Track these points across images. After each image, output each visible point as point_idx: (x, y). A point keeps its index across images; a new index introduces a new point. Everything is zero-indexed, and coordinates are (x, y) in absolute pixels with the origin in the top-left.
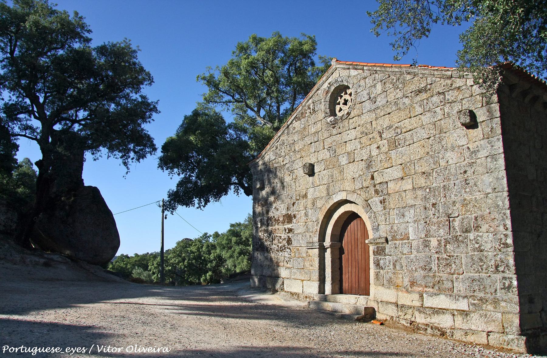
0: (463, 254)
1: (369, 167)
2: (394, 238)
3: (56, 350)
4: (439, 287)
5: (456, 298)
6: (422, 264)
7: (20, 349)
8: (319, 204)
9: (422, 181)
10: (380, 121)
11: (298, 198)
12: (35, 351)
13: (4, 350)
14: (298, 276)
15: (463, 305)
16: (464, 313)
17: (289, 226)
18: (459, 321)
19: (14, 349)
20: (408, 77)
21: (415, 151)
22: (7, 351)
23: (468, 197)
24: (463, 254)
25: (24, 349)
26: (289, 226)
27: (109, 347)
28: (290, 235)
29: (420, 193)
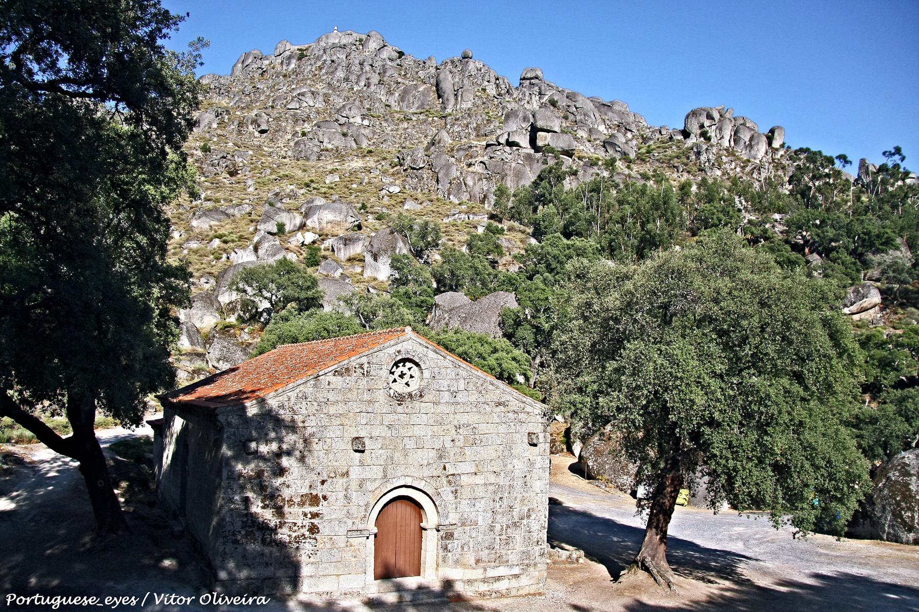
0: (518, 535)
1: (440, 457)
2: (463, 524)
3: (90, 600)
4: (500, 560)
5: (511, 566)
6: (487, 545)
7: (33, 600)
8: (370, 486)
9: (492, 478)
10: (458, 416)
11: (333, 475)
12: (57, 602)
13: (9, 600)
14: (332, 570)
15: (516, 570)
16: (516, 576)
17: (314, 509)
18: (514, 583)
19: (24, 599)
20: (491, 387)
21: (489, 453)
22: (13, 603)
23: (526, 495)
24: (518, 535)
25: (39, 600)
26: (314, 509)
27: (173, 596)
28: (316, 521)
29: (491, 488)
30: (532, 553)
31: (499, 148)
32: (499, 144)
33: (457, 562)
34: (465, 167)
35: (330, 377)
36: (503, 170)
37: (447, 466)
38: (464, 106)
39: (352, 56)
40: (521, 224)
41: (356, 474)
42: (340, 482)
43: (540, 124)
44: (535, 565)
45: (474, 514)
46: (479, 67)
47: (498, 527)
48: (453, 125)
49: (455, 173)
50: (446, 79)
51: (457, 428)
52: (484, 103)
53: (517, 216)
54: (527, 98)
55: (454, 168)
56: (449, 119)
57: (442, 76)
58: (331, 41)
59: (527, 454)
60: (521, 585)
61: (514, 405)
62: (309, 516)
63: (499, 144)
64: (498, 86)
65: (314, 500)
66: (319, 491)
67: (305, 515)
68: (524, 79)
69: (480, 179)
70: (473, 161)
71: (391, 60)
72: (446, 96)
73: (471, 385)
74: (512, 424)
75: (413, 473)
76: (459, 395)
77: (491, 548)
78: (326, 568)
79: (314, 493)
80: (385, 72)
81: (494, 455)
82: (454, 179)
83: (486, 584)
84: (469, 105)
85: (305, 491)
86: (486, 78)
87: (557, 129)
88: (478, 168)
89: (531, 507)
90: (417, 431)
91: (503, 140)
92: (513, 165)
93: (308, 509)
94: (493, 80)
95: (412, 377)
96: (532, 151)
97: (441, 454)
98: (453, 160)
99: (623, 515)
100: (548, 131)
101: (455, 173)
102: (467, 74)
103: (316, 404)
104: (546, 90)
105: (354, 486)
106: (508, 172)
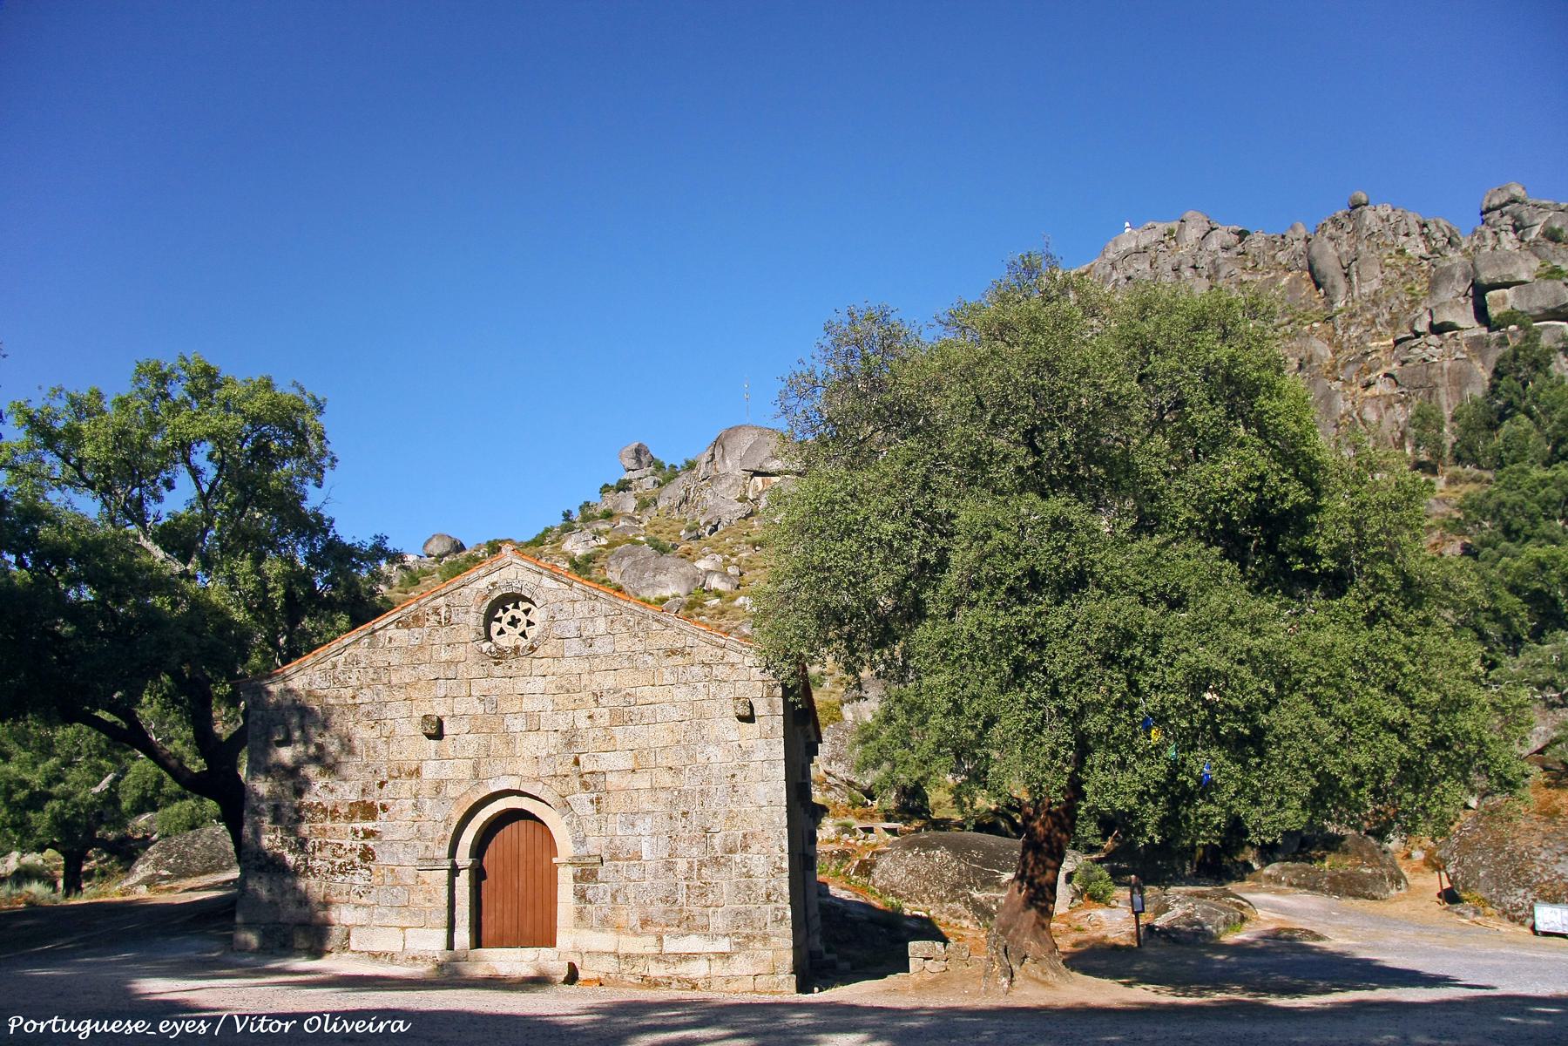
0: (724, 883)
1: (569, 744)
2: (614, 857)
4: (687, 924)
5: (714, 937)
9: (666, 779)
10: (598, 677)
14: (393, 919)
15: (723, 945)
16: (725, 956)
17: (369, 825)
18: (718, 968)
20: (656, 626)
21: (658, 735)
24: (724, 883)
26: (369, 825)
28: (370, 843)
29: (663, 795)
30: (756, 915)
31: (1415, 342)
32: (1418, 335)
33: (605, 923)
34: (1360, 391)
35: (392, 631)
36: (1429, 379)
37: (582, 758)
38: (1366, 290)
39: (1160, 261)
40: (1479, 467)
41: (430, 771)
42: (407, 785)
43: (1486, 276)
44: (765, 938)
45: (632, 839)
46: (1383, 214)
47: (682, 865)
48: (1346, 329)
49: (1342, 406)
50: (1323, 253)
51: (596, 697)
52: (1403, 274)
53: (1466, 454)
54: (1490, 242)
55: (1340, 397)
56: (1339, 319)
57: (1315, 251)
58: (1123, 247)
59: (733, 736)
60: (737, 972)
61: (705, 652)
62: (361, 834)
63: (1418, 335)
64: (1427, 238)
65: (369, 811)
66: (375, 798)
67: (356, 833)
68: (1489, 210)
69: (1389, 406)
70: (1372, 376)
71: (1226, 249)
72: (1329, 281)
73: (617, 626)
74: (699, 685)
75: (523, 767)
76: (598, 643)
77: (669, 899)
78: (385, 915)
79: (369, 800)
80: (1217, 271)
81: (669, 739)
82: (1342, 417)
83: (662, 965)
84: (1376, 284)
85: (354, 797)
86: (1402, 229)
87: (1524, 277)
88: (1382, 388)
89: (749, 830)
90: (529, 705)
91: (1421, 327)
92: (1447, 364)
93: (360, 825)
94: (1415, 229)
95: (529, 623)
96: (1484, 331)
97: (570, 739)
98: (1338, 384)
99: (1383, 950)
100: (1507, 285)
101: (1342, 406)
102: (1364, 233)
103: (371, 671)
104: (1532, 217)
105: (427, 790)
106: (1439, 381)
